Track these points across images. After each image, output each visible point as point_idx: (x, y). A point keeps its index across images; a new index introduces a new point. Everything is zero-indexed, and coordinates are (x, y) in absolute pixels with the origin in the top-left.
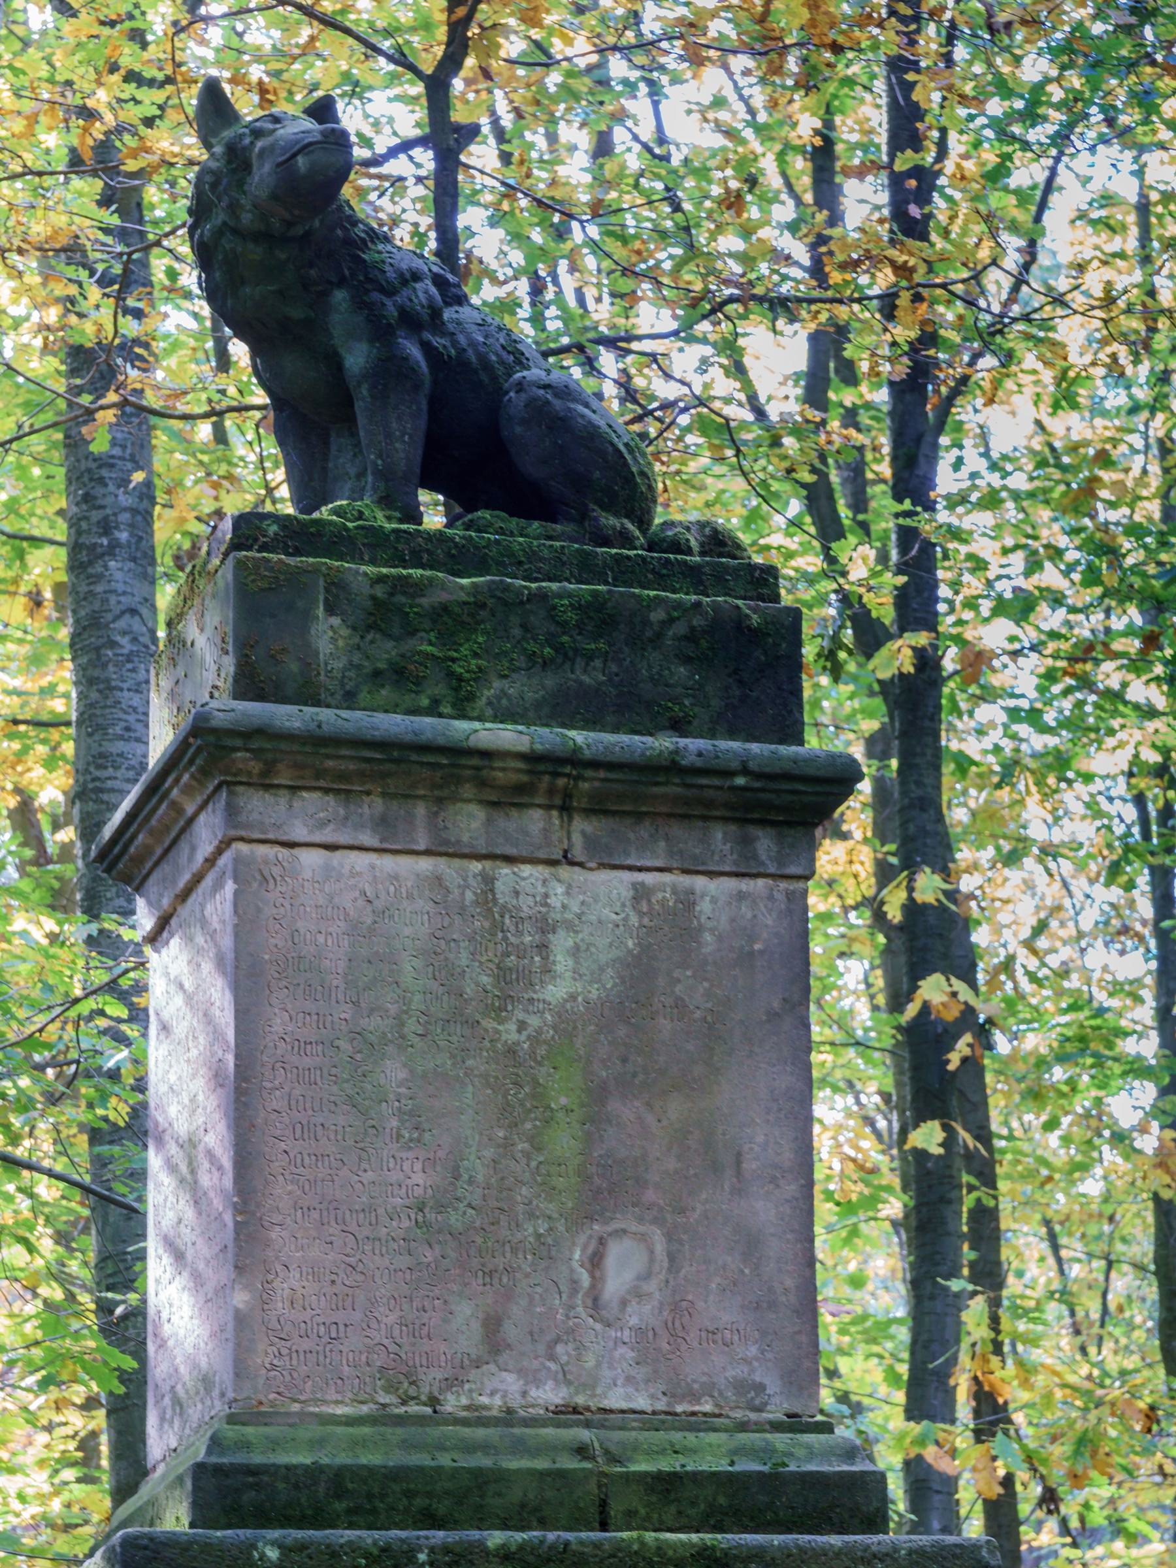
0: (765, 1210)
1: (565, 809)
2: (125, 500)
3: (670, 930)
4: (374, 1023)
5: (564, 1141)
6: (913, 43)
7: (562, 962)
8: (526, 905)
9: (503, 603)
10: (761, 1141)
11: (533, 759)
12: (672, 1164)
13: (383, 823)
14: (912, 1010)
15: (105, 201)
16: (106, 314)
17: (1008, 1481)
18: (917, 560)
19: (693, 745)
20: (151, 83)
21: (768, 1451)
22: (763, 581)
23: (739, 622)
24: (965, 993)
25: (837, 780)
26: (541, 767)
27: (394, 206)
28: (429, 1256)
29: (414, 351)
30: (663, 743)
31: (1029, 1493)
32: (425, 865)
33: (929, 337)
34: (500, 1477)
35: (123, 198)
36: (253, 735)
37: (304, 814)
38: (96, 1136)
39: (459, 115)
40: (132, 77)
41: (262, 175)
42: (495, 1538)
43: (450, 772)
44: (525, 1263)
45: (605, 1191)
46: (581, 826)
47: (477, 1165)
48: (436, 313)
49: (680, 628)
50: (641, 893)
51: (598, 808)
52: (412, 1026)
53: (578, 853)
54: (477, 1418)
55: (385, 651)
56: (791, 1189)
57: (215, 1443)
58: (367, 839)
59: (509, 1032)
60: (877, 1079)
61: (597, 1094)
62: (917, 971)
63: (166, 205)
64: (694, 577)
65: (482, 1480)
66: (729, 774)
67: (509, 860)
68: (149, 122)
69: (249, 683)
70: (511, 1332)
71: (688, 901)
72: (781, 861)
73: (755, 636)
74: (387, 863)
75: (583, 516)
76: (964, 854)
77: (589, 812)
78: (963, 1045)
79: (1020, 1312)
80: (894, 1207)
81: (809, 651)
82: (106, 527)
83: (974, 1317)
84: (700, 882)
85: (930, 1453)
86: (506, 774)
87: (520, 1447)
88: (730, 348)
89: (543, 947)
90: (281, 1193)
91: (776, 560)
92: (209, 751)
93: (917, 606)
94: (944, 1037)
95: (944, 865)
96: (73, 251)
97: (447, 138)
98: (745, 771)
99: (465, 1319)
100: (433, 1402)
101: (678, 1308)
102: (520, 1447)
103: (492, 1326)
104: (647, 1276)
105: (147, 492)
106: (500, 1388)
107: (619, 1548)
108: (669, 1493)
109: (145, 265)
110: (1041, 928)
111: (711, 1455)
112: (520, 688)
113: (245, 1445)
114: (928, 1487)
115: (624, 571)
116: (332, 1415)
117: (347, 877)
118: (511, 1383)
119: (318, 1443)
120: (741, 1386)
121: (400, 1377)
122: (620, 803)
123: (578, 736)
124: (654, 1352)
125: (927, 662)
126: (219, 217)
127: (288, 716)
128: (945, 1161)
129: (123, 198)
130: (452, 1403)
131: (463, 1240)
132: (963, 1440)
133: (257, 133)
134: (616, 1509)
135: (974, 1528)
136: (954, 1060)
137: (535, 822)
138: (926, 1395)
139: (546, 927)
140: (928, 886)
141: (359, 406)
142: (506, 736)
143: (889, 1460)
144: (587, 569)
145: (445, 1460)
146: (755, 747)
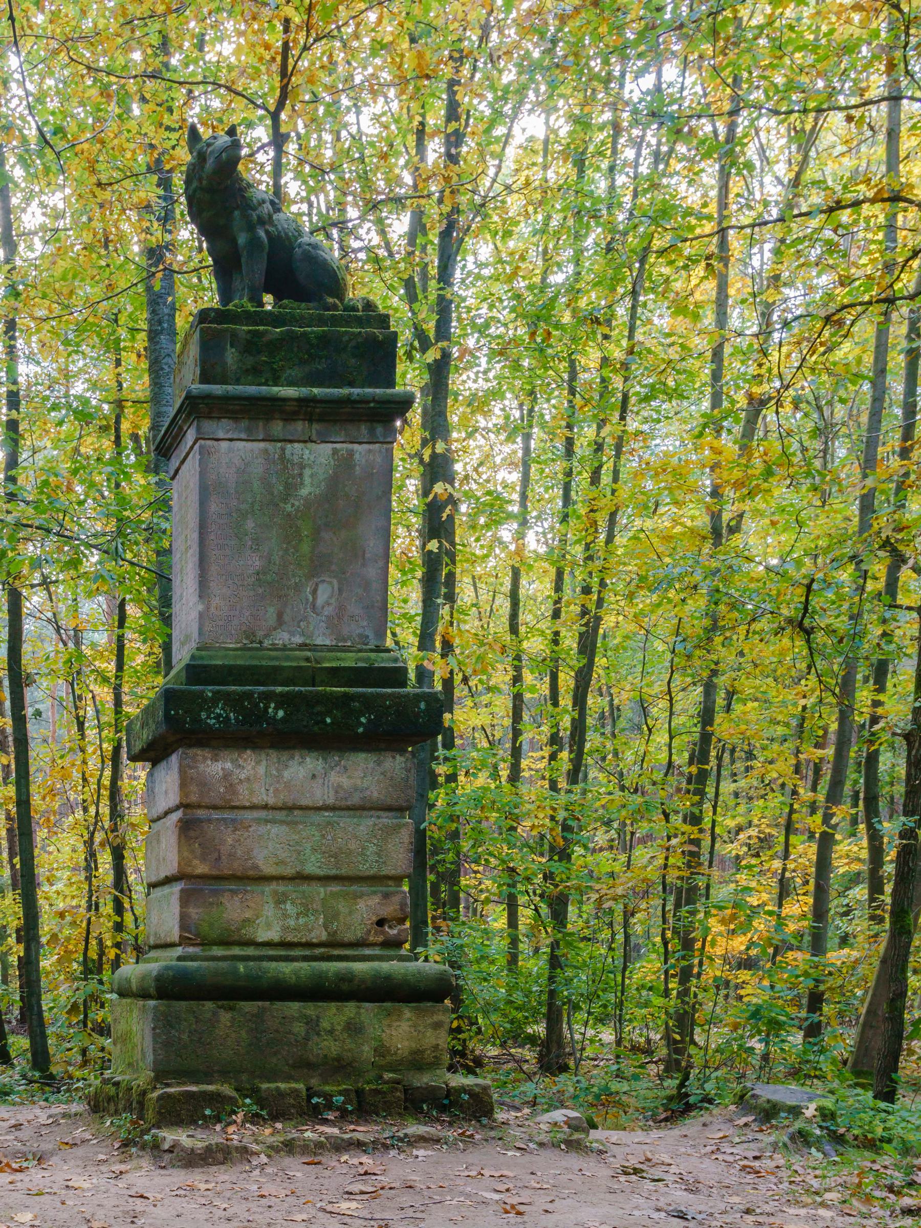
0: (372, 572)
1: (311, 421)
2: (166, 311)
3: (345, 463)
4: (243, 506)
5: (305, 548)
6: (458, 71)
7: (307, 480)
8: (296, 459)
9: (291, 338)
10: (372, 545)
11: (300, 400)
12: (341, 555)
13: (249, 430)
14: (431, 497)
15: (158, 185)
16: (159, 234)
17: (451, 672)
18: (444, 308)
20: (174, 130)
21: (369, 659)
22: (384, 320)
23: (375, 336)
24: (450, 490)
25: (404, 404)
27: (257, 174)
28: (260, 591)
29: (262, 234)
30: (345, 391)
31: (458, 678)
32: (262, 445)
33: (456, 210)
35: (165, 183)
36: (207, 397)
37: (222, 428)
38: (158, 553)
39: (283, 130)
40: (168, 128)
41: (210, 164)
42: (279, 689)
44: (292, 593)
45: (318, 566)
46: (315, 426)
47: (276, 558)
48: (270, 217)
49: (353, 343)
50: (335, 452)
51: (322, 419)
52: (257, 507)
53: (314, 438)
54: (274, 648)
55: (250, 361)
56: (381, 564)
57: (193, 657)
58: (243, 436)
59: (289, 508)
60: (416, 521)
62: (433, 481)
63: (178, 182)
64: (359, 321)
65: (276, 669)
66: (368, 402)
67: (291, 441)
68: (173, 148)
69: (205, 378)
70: (286, 618)
71: (351, 453)
72: (385, 436)
73: (381, 343)
74: (249, 445)
75: (321, 298)
76: (455, 435)
77: (318, 421)
78: (447, 511)
79: (463, 612)
80: (419, 574)
81: (401, 352)
82: (160, 322)
83: (445, 611)
84: (356, 447)
85: (425, 663)
87: (288, 658)
88: (380, 222)
89: (301, 475)
90: (214, 569)
91: (391, 312)
92: (197, 408)
93: (443, 330)
94: (441, 508)
95: (446, 440)
96: (148, 207)
97: (279, 140)
98: (374, 400)
100: (261, 642)
101: (341, 608)
102: (288, 658)
103: (280, 615)
104: (331, 597)
105: (173, 308)
106: (282, 637)
107: (318, 692)
108: (336, 675)
109: (173, 211)
110: (481, 464)
111: (349, 661)
112: (295, 372)
113: (202, 658)
114: (423, 675)
115: (335, 321)
116: (229, 649)
117: (236, 452)
118: (286, 636)
119: (225, 657)
120: (361, 636)
121: (250, 634)
123: (315, 390)
124: (333, 624)
125: (446, 355)
126: (195, 184)
127: (217, 389)
128: (438, 555)
129: (165, 183)
130: (267, 643)
131: (273, 586)
132: (437, 656)
133: (209, 145)
134: (318, 679)
135: (438, 687)
136: (445, 516)
137: (299, 426)
138: (425, 641)
140: (440, 447)
141: (243, 260)
142: (290, 392)
143: (411, 667)
144: (321, 321)
145: (264, 663)
146: (378, 391)
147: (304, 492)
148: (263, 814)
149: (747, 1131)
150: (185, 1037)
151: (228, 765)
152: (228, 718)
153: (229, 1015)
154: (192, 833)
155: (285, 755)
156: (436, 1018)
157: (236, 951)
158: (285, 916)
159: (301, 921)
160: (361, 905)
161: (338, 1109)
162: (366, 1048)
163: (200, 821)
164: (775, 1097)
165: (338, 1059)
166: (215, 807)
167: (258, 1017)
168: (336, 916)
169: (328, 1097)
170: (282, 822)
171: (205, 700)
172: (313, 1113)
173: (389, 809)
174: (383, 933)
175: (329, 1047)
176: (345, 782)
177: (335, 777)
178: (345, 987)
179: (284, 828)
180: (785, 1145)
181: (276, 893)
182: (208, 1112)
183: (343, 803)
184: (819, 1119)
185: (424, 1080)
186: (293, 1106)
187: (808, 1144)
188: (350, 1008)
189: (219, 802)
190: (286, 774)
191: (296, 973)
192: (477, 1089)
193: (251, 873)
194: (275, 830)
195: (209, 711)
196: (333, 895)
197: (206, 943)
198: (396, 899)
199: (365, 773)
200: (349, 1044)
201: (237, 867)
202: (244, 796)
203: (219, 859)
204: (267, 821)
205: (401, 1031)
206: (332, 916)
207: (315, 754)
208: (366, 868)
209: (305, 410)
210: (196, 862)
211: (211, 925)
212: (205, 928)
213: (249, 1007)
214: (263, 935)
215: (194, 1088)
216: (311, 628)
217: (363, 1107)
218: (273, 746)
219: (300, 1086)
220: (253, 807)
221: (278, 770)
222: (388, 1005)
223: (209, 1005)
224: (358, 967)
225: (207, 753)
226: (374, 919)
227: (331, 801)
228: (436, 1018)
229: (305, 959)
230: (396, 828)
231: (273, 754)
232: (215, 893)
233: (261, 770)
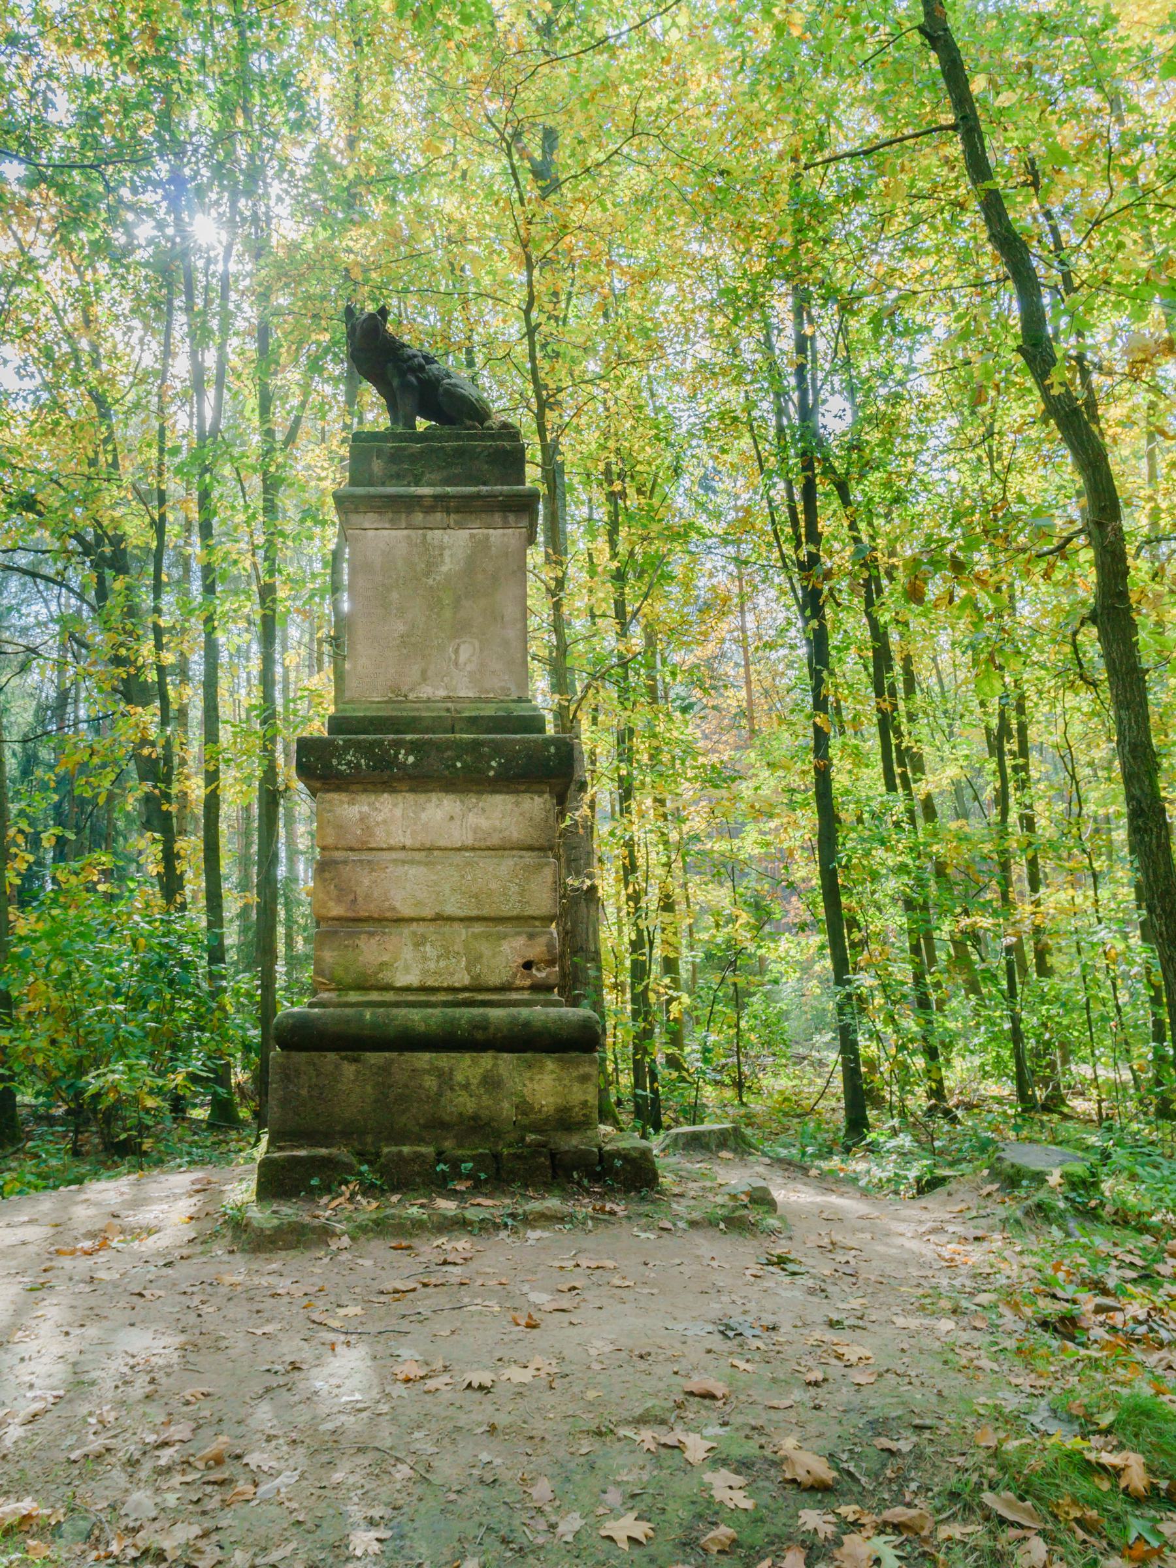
1: (448, 513)
5: (448, 614)
7: (447, 559)
9: (432, 450)
10: (510, 611)
11: (435, 497)
19: (484, 489)
25: (533, 496)
26: (838, 556)
34: (421, 718)
42: (409, 737)
43: (409, 504)
45: (460, 629)
50: (472, 536)
51: (457, 511)
54: (418, 700)
55: (395, 468)
61: (458, 600)
65: (415, 719)
71: (487, 538)
86: (427, 502)
99: (415, 671)
103: (424, 672)
106: (426, 691)
108: (474, 723)
111: (489, 711)
112: (434, 476)
117: (385, 538)
121: (396, 690)
122: (465, 508)
130: (411, 696)
139: (442, 548)
144: (459, 437)
147: (445, 569)
148: (401, 855)
149: (989, 1202)
150: (304, 1092)
151: (365, 809)
152: (358, 765)
153: (353, 1068)
154: (327, 875)
155: (422, 798)
156: (583, 1070)
157: (374, 996)
158: (425, 959)
159: (442, 964)
160: (505, 947)
161: (468, 1177)
162: (506, 1105)
163: (336, 862)
164: (1020, 1161)
165: (475, 1118)
166: (352, 849)
167: (385, 1069)
168: (479, 958)
169: (455, 1163)
170: (419, 863)
171: (337, 748)
172: (440, 1185)
173: (530, 848)
174: (530, 976)
175: (466, 1103)
176: (484, 823)
177: (473, 819)
178: (479, 1035)
179: (423, 870)
180: (1017, 1222)
181: (414, 934)
182: (315, 1182)
183: (483, 844)
184: (1065, 1188)
185: (574, 1142)
186: (419, 1174)
187: (1048, 1220)
188: (486, 1060)
189: (354, 844)
190: (423, 816)
191: (425, 1019)
192: (635, 1154)
193: (388, 914)
194: (412, 871)
195: (340, 757)
196: (475, 936)
197: (342, 988)
198: (543, 940)
199: (507, 814)
200: (486, 1101)
201: (372, 909)
202: (380, 838)
203: (355, 901)
204: (404, 862)
205: (544, 1085)
206: (474, 959)
207: (452, 797)
208: (506, 910)
209: (440, 503)
210: (331, 904)
211: (346, 969)
212: (339, 973)
213: (374, 1058)
214: (401, 980)
215: (302, 1153)
216: (454, 681)
217: (498, 1175)
219: (427, 1150)
220: (390, 849)
222: (528, 1055)
223: (332, 1056)
224: (496, 1014)
225: (344, 797)
226: (521, 961)
227: (470, 842)
228: (583, 1070)
229: (446, 1004)
230: (539, 868)
231: (410, 797)
232: (350, 935)
233: (398, 812)
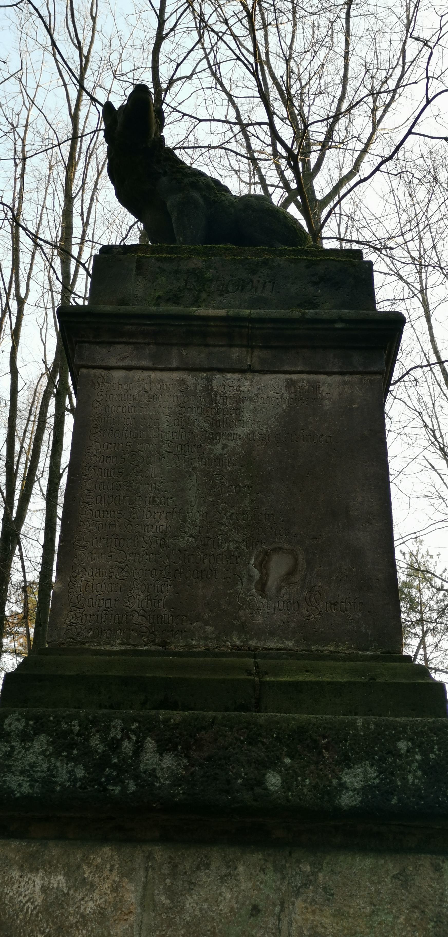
7: (246, 415)
32: (176, 375)
50: (290, 384)
58: (145, 363)
59: (218, 449)
71: (315, 387)
147: (240, 431)
207: (257, 857)
209: (233, 330)
218: (167, 838)
221: (171, 893)
233: (131, 895)
